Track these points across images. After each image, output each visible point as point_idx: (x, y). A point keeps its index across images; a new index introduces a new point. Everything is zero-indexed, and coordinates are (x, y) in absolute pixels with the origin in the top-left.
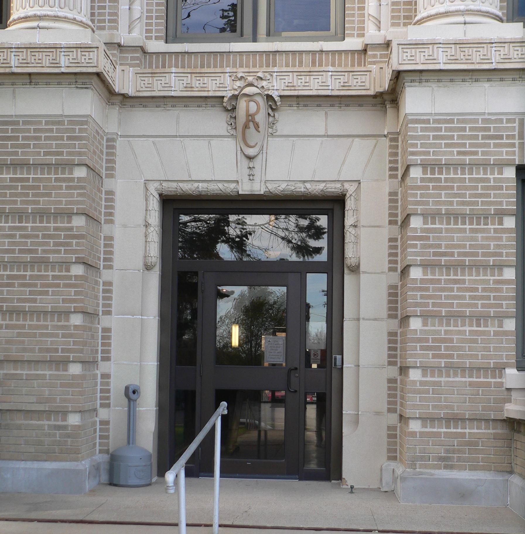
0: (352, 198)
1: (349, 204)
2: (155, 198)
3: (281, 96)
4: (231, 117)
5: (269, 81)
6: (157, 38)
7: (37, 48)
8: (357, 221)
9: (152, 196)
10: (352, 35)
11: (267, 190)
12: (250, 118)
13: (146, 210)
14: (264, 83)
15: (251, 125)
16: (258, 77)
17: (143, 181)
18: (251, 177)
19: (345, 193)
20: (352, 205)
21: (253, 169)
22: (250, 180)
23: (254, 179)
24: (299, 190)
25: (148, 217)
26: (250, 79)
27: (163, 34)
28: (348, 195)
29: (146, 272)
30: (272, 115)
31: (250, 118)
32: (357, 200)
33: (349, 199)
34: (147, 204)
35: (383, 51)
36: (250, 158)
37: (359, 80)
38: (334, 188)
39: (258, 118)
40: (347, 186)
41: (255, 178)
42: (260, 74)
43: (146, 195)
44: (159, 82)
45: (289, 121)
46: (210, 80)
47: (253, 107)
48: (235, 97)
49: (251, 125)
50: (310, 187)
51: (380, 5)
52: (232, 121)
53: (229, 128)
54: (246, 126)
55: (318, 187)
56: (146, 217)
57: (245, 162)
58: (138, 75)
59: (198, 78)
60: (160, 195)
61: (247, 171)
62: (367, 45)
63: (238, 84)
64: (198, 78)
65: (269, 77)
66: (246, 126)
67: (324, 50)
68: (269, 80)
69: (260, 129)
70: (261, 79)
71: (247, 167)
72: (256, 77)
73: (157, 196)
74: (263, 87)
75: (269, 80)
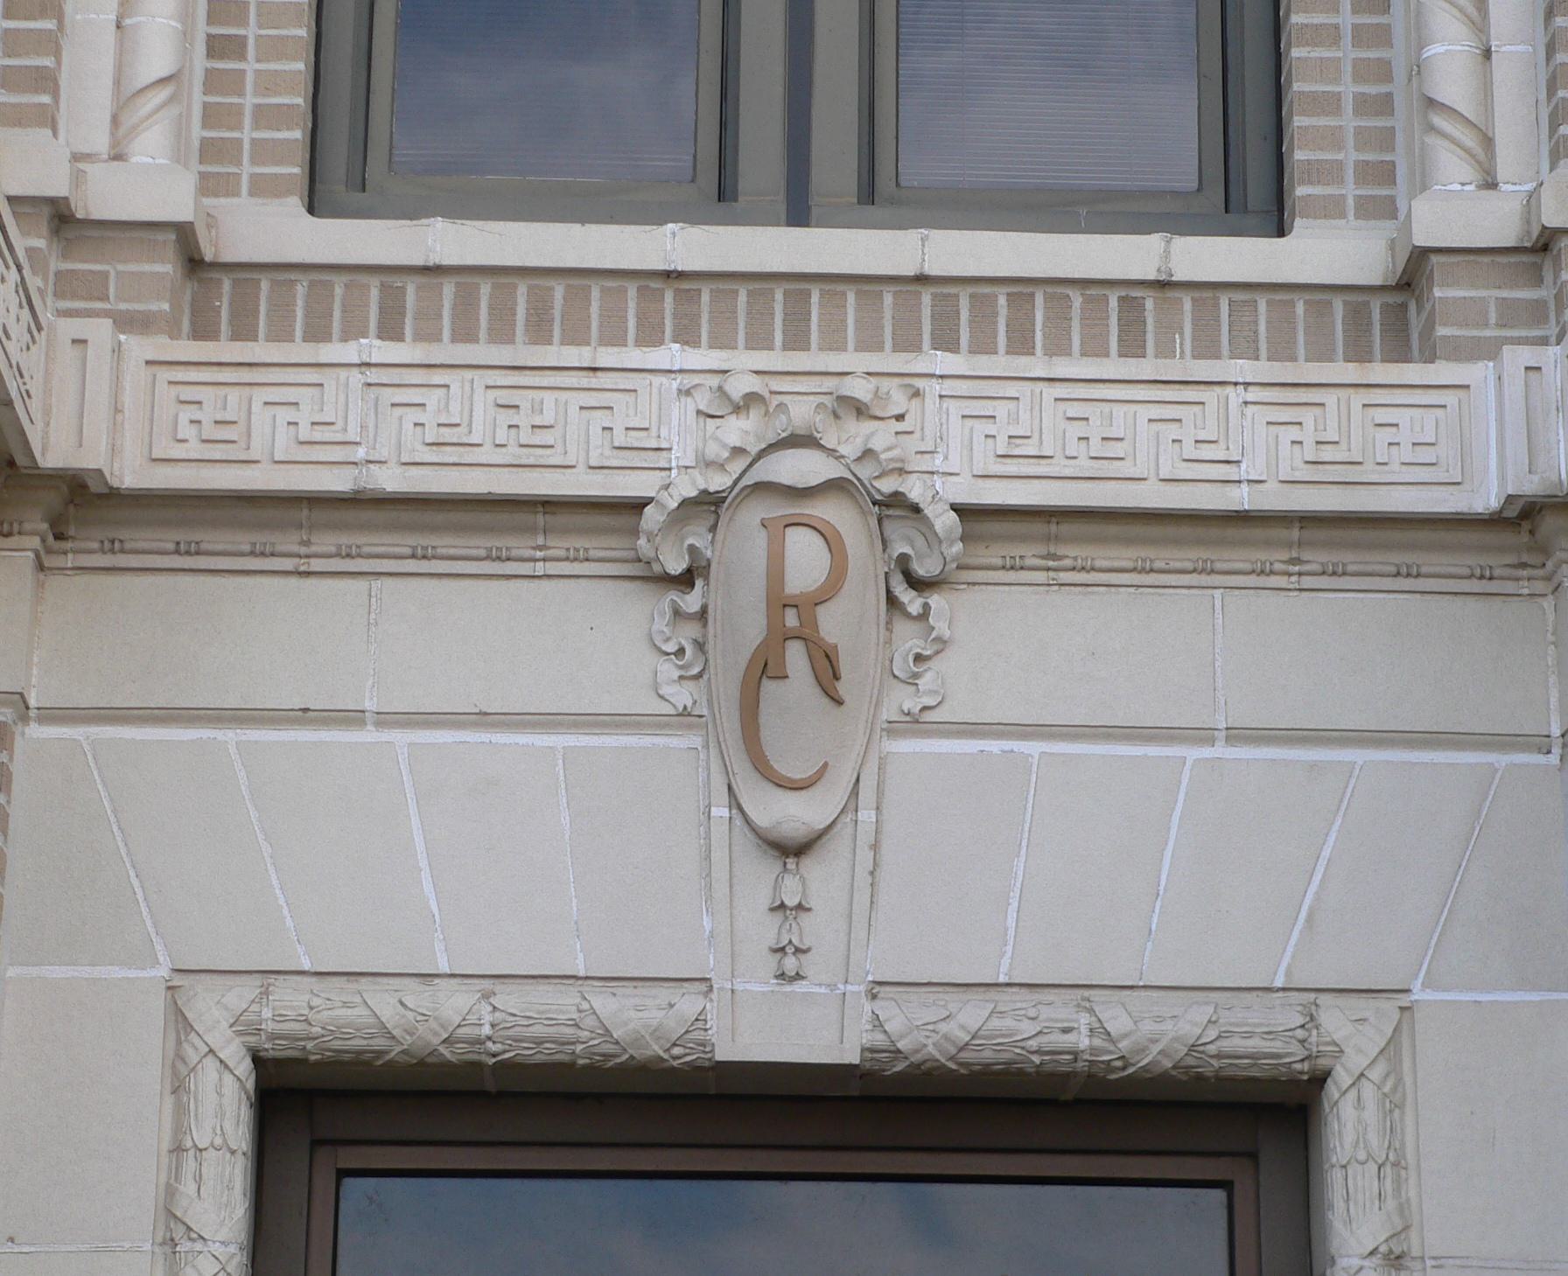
0: (1368, 1090)
1: (1349, 1127)
2: (228, 1079)
3: (963, 511)
4: (677, 613)
5: (900, 426)
6: (263, 188)
7: (1415, 1072)
8: (1406, 1228)
9: (210, 1063)
10: (1331, 209)
11: (879, 1039)
12: (793, 625)
13: (178, 1149)
14: (881, 436)
15: (796, 656)
16: (842, 399)
17: (163, 972)
18: (790, 964)
19: (1323, 1062)
20: (1373, 1139)
21: (803, 916)
22: (781, 976)
23: (807, 971)
24: (1068, 1040)
25: (189, 1187)
26: (801, 413)
27: (295, 170)
28: (1342, 1076)
29: (41, 576)
30: (915, 608)
31: (793, 625)
32: (1393, 1104)
33: (1352, 1094)
34: (180, 1111)
35: (1514, 286)
36: (791, 850)
37: (1405, 437)
38: (1256, 1036)
39: (832, 624)
40: (1335, 1021)
41: (810, 964)
42: (860, 389)
43: (180, 1056)
44: (284, 415)
45: (1010, 641)
46: (573, 410)
47: (806, 561)
48: (708, 504)
49: (796, 656)
50: (1129, 1025)
51: (1487, 54)
52: (686, 634)
53: (668, 670)
54: (764, 668)
55: (1168, 1026)
56: (171, 1192)
57: (760, 878)
58: (165, 374)
59: (1074, 410)
60: (259, 1061)
61: (768, 930)
62: (1421, 256)
63: (738, 430)
64: (1074, 410)
65: (899, 402)
66: (764, 668)
67: (1178, 276)
68: (900, 418)
69: (842, 688)
70: (860, 410)
71: (764, 899)
72: (826, 400)
73: (245, 1068)
74: (868, 454)
75: (900, 418)
